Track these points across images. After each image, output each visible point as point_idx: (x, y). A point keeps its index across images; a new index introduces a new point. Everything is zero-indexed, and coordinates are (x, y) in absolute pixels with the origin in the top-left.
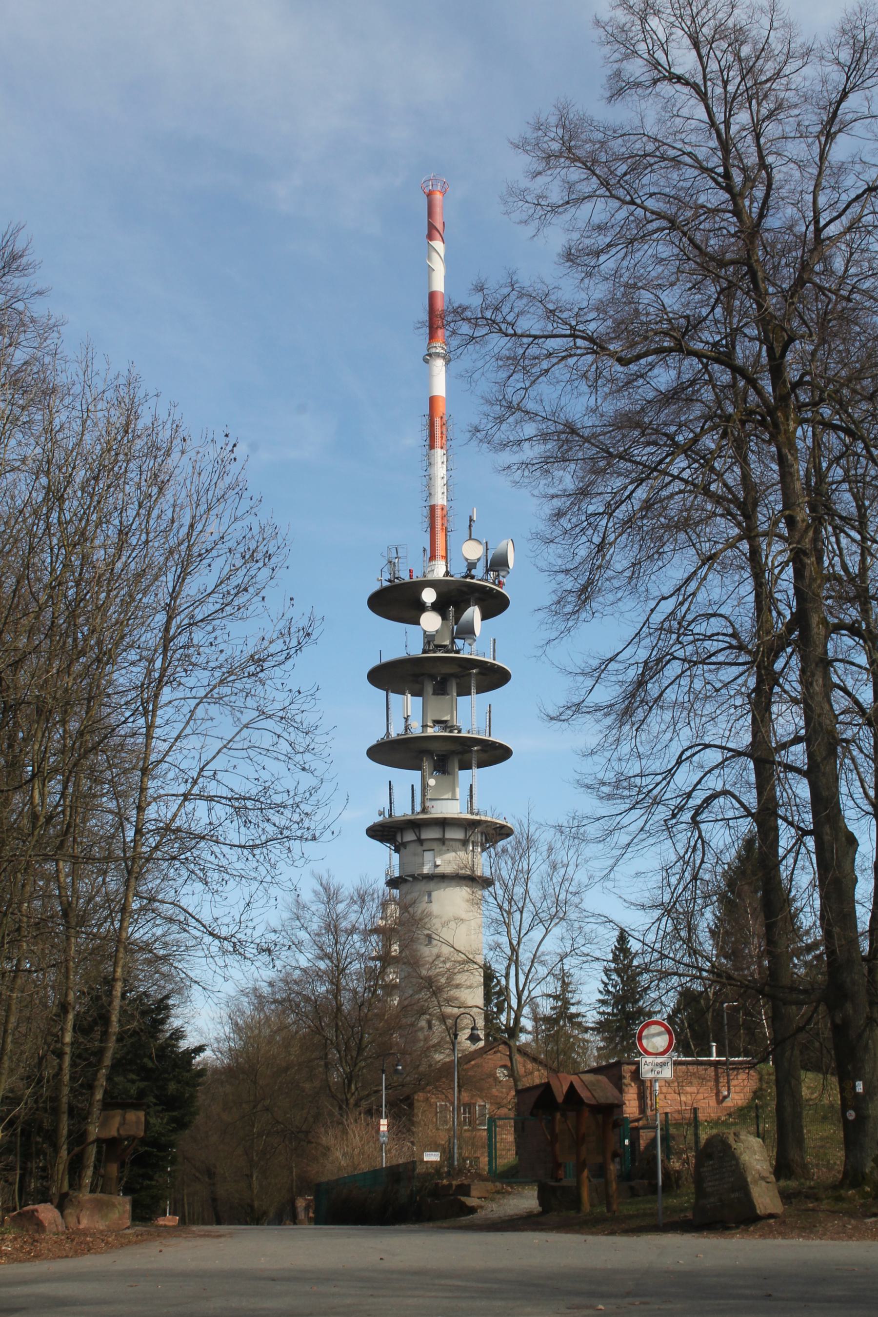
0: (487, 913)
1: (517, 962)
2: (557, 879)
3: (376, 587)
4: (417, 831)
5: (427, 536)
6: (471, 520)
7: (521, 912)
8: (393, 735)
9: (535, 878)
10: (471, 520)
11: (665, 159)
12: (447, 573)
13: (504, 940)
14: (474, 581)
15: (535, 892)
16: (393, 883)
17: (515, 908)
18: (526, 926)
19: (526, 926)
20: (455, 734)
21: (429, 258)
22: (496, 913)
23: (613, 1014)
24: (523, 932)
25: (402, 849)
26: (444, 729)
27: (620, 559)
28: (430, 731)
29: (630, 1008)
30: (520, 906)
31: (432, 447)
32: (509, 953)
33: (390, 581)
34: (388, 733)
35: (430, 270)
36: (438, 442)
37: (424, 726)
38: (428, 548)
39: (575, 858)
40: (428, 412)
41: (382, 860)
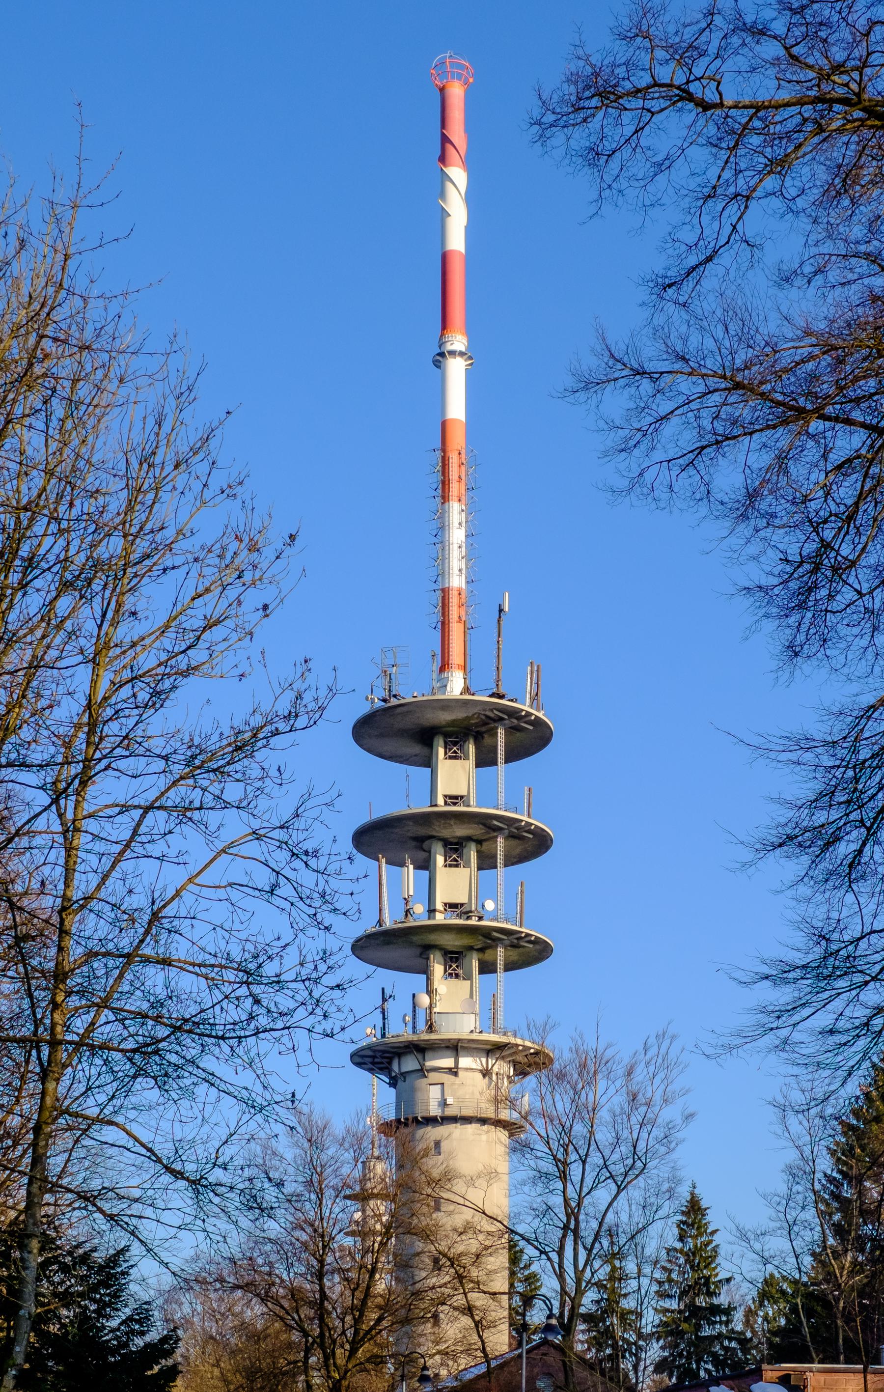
0: (532, 1163)
1: (576, 1232)
2: (635, 1119)
3: (365, 709)
4: (420, 1056)
5: (438, 634)
6: (501, 610)
7: (584, 1162)
8: (388, 924)
9: (604, 1114)
10: (501, 610)
11: (217, 769)
12: (467, 690)
13: (557, 1201)
14: (504, 702)
15: (603, 1136)
16: (386, 1128)
17: (573, 1157)
18: (588, 1182)
19: (588, 1182)
20: (474, 922)
21: (442, 194)
22: (548, 1166)
23: (680, 1312)
24: (585, 1190)
25: (400, 1083)
26: (460, 916)
27: (419, 909)
28: (440, 918)
29: (701, 1301)
30: (583, 1152)
31: (445, 498)
32: (565, 1219)
33: (385, 700)
34: (380, 922)
35: (444, 214)
36: (455, 488)
37: (432, 911)
38: (438, 652)
39: (663, 1087)
40: (439, 445)
41: (377, 1097)
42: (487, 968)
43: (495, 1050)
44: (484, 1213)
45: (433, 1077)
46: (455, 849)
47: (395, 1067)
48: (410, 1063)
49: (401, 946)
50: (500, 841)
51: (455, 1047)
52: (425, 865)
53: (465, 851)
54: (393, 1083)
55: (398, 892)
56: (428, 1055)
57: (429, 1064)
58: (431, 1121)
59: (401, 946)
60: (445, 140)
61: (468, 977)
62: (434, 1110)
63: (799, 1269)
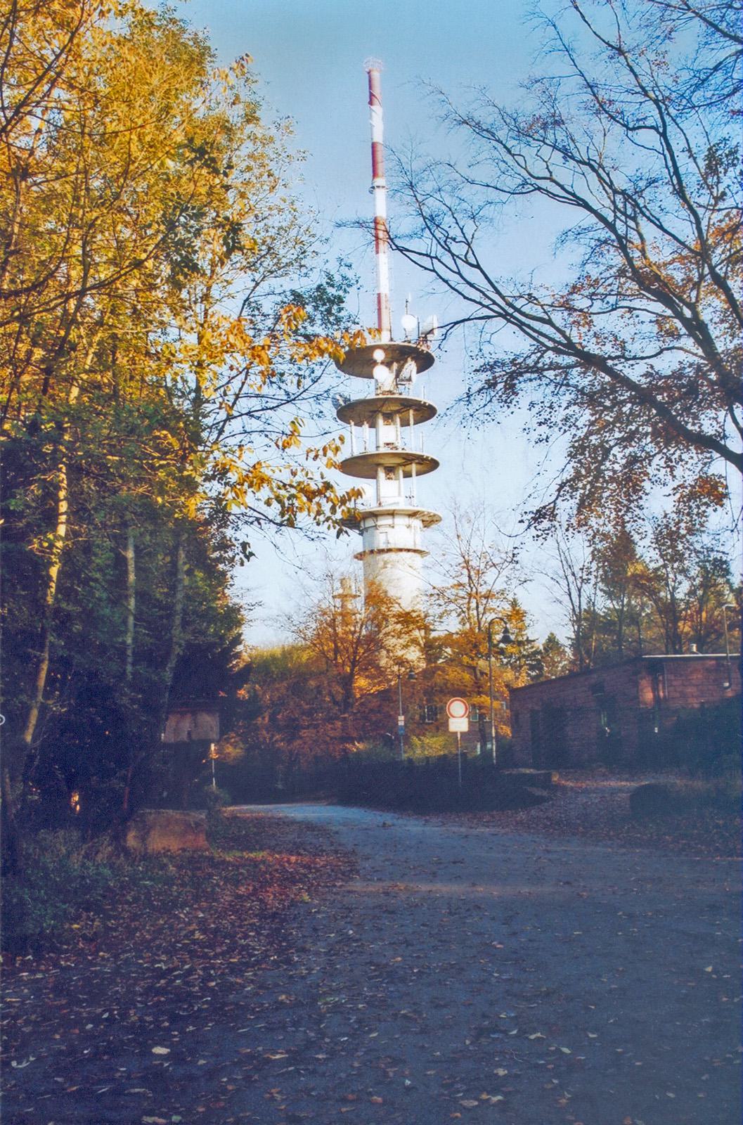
21: (371, 117)
28: (383, 450)
42: (407, 475)
43: (413, 515)
44: (462, 229)
45: (381, 529)
46: (389, 417)
47: (362, 524)
48: (370, 523)
49: (361, 466)
50: (411, 412)
51: (392, 514)
52: (373, 425)
53: (278, 652)
54: (361, 534)
55: (360, 440)
56: (379, 518)
57: (379, 523)
58: (381, 551)
59: (361, 466)
60: (372, 95)
61: (397, 479)
62: (382, 546)
63: (490, 401)
